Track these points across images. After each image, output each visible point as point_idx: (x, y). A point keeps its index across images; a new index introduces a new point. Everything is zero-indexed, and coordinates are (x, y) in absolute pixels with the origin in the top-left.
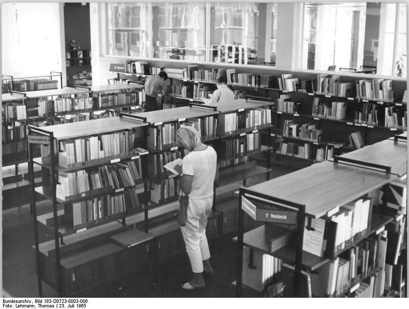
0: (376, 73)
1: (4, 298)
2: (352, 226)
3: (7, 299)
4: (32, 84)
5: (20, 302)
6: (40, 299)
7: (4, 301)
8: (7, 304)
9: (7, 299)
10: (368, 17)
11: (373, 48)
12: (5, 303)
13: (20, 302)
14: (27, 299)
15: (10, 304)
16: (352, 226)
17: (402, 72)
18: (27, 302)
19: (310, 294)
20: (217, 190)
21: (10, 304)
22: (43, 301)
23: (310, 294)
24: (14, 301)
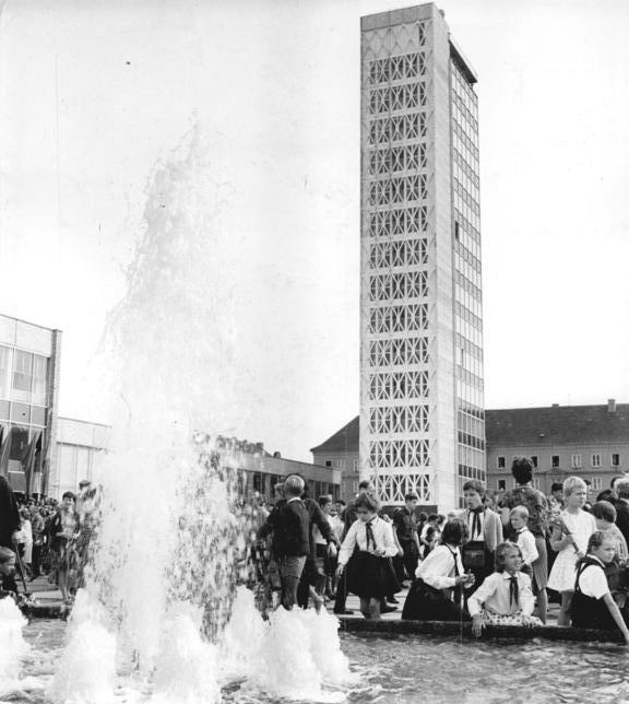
17: (450, 230)
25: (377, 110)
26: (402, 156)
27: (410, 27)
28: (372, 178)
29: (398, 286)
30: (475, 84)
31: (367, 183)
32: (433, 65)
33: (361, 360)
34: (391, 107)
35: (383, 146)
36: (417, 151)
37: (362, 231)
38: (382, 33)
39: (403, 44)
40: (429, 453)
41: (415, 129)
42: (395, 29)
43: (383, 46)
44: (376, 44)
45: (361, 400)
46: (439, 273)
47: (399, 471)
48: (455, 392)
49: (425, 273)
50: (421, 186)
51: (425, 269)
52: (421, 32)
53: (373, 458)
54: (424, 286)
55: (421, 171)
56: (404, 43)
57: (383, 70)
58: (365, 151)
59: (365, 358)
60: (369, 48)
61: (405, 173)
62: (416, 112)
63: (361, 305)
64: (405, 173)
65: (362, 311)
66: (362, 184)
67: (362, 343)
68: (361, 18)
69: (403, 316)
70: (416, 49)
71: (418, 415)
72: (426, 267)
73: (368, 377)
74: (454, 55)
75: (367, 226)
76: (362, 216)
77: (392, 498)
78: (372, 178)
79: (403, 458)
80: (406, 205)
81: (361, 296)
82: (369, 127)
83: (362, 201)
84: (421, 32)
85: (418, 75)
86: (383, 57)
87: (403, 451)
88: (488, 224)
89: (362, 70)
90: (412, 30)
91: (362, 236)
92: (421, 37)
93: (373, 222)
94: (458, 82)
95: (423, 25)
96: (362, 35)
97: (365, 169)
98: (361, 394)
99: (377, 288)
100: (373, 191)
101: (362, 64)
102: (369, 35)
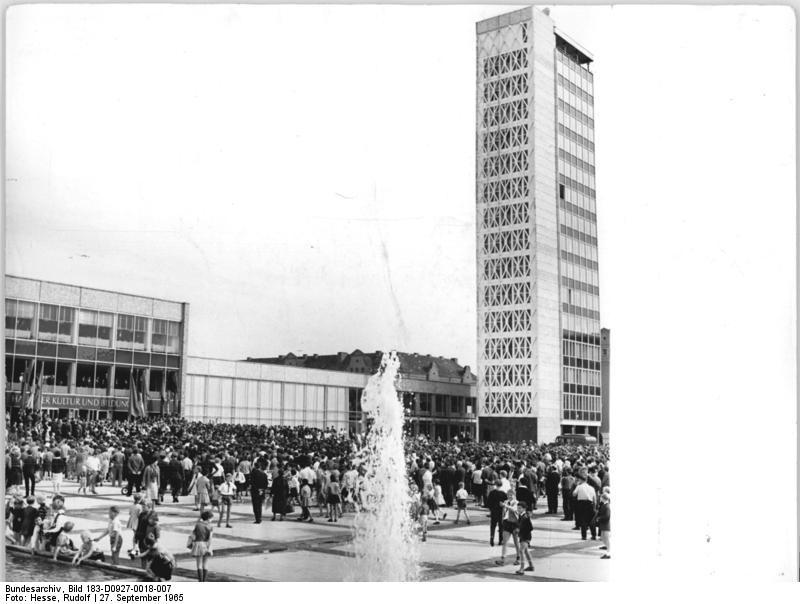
0: (592, 518)
1: (8, 583)
2: (249, 360)
3: (13, 585)
4: (592, 354)
5: (39, 590)
6: (79, 584)
7: (8, 588)
8: (14, 594)
9: (13, 585)
10: (571, 426)
11: (287, 362)
12: (10, 593)
13: (39, 590)
14: (52, 584)
15: (19, 594)
16: (249, 360)
17: (553, 193)
18: (54, 590)
19: (150, 323)
20: (342, 391)
21: (19, 594)
22: (85, 589)
23: (150, 323)
24: (28, 589)
25: (489, 200)
26: (508, 136)
27: (517, 26)
28: (485, 155)
29: (505, 242)
30: (591, 63)
31: (481, 160)
32: (533, 59)
33: (478, 301)
34: (501, 223)
35: (494, 129)
36: (520, 106)
37: (477, 199)
38: (493, 34)
39: (509, 44)
40: (530, 347)
41: (522, 296)
42: (502, 31)
43: (494, 45)
44: (488, 43)
45: (478, 306)
46: (538, 230)
47: (507, 389)
48: (556, 119)
49: (527, 230)
50: (523, 159)
51: (529, 335)
52: (524, 31)
53: (487, 379)
54: (527, 295)
55: (523, 147)
56: (510, 41)
57: (494, 66)
58: (480, 134)
59: (480, 300)
60: (483, 48)
61: (510, 150)
62: (520, 202)
63: (477, 258)
64: (510, 150)
65: (478, 263)
66: (477, 161)
67: (478, 288)
68: (477, 23)
69: (511, 401)
70: (521, 46)
71: (523, 372)
72: (527, 226)
73: (482, 236)
74: (561, 43)
75: (481, 195)
76: (477, 187)
77: (503, 411)
78: (485, 155)
79: (511, 379)
80: (511, 175)
81: (477, 251)
82: (483, 64)
83: (477, 174)
84: (524, 31)
85: (523, 171)
86: (494, 54)
87: (511, 373)
88: (603, 183)
89: (477, 67)
90: (517, 30)
91: (477, 202)
92: (524, 35)
93: (486, 140)
94: (567, 68)
95: (525, 25)
96: (478, 38)
97: (479, 148)
98: (478, 328)
99: (489, 244)
100: (486, 165)
101: (477, 62)
102: (482, 37)
